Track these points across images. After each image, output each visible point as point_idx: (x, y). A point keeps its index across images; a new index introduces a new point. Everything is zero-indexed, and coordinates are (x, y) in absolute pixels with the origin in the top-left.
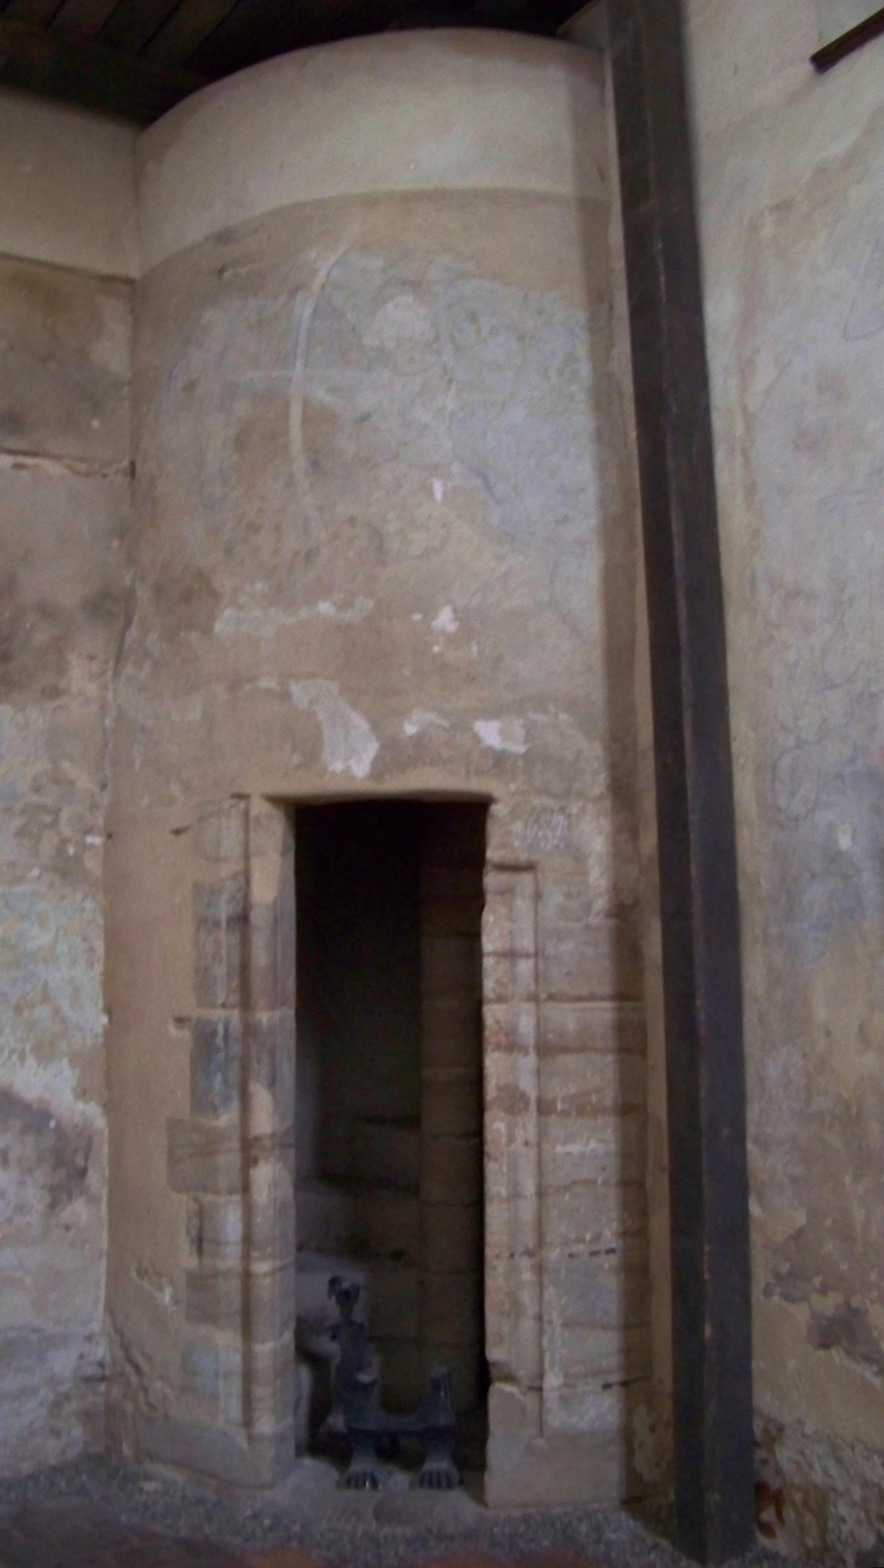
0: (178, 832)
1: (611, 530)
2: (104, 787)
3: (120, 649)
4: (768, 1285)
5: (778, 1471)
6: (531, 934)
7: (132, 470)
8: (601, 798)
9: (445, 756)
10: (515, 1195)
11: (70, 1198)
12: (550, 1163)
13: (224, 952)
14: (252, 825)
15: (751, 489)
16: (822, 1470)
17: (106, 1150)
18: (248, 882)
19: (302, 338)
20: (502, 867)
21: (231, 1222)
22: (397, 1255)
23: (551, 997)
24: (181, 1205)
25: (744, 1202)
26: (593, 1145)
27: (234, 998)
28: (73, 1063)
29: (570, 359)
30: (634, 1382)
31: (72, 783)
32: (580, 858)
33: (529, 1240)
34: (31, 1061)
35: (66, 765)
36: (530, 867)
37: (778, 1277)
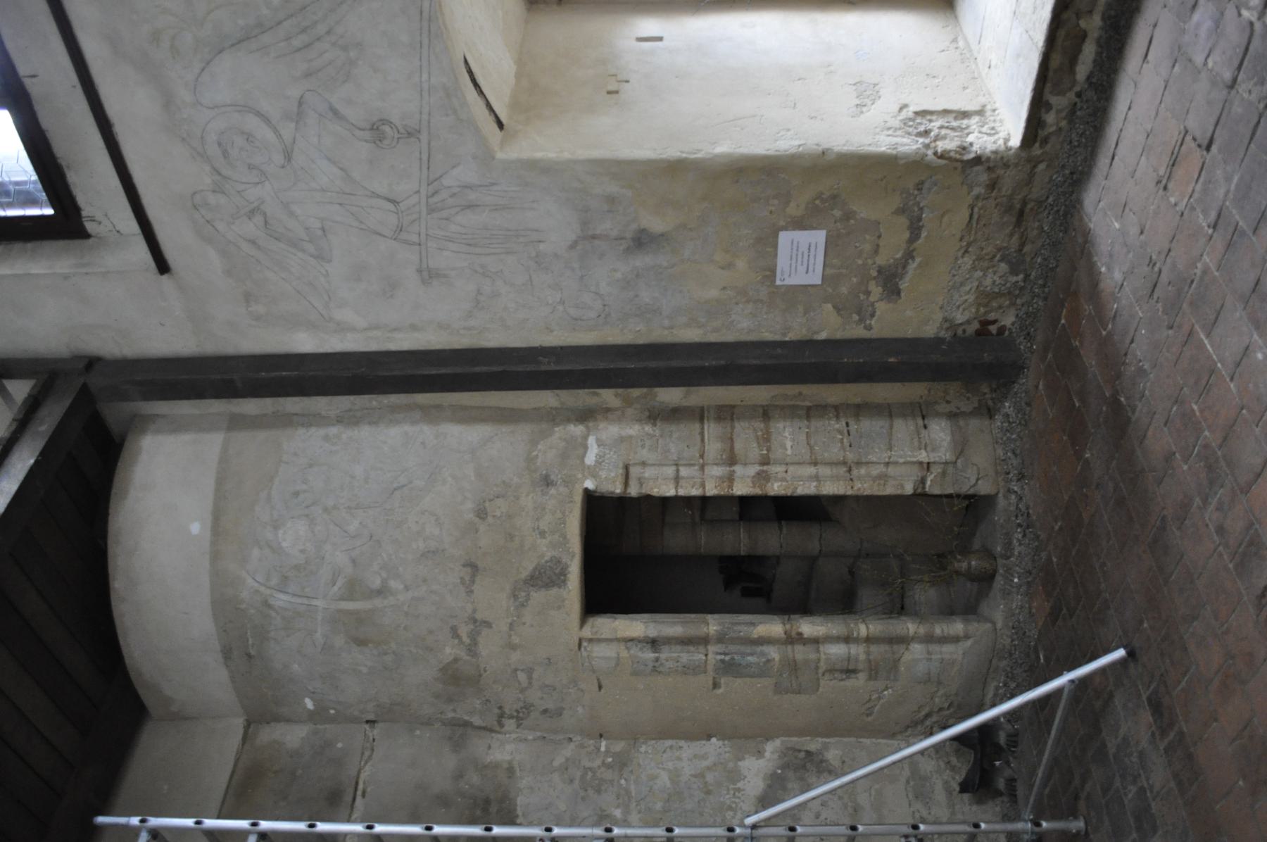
0: (600, 687)
1: (431, 415)
2: (570, 739)
3: (485, 728)
4: (865, 328)
5: (968, 322)
6: (665, 468)
7: (371, 722)
8: (587, 428)
9: (559, 515)
10: (817, 478)
11: (826, 761)
12: (798, 457)
13: (675, 655)
14: (598, 636)
15: (414, 328)
16: (967, 295)
17: (795, 739)
18: (632, 640)
19: (299, 600)
20: (626, 484)
21: (836, 651)
22: (851, 573)
23: (702, 456)
24: (828, 685)
25: (817, 341)
26: (787, 434)
27: (702, 649)
28: (743, 759)
29: (326, 438)
30: (921, 411)
31: (567, 760)
32: (622, 439)
33: (843, 470)
34: (740, 785)
35: (556, 764)
36: (627, 468)
37: (861, 320)
